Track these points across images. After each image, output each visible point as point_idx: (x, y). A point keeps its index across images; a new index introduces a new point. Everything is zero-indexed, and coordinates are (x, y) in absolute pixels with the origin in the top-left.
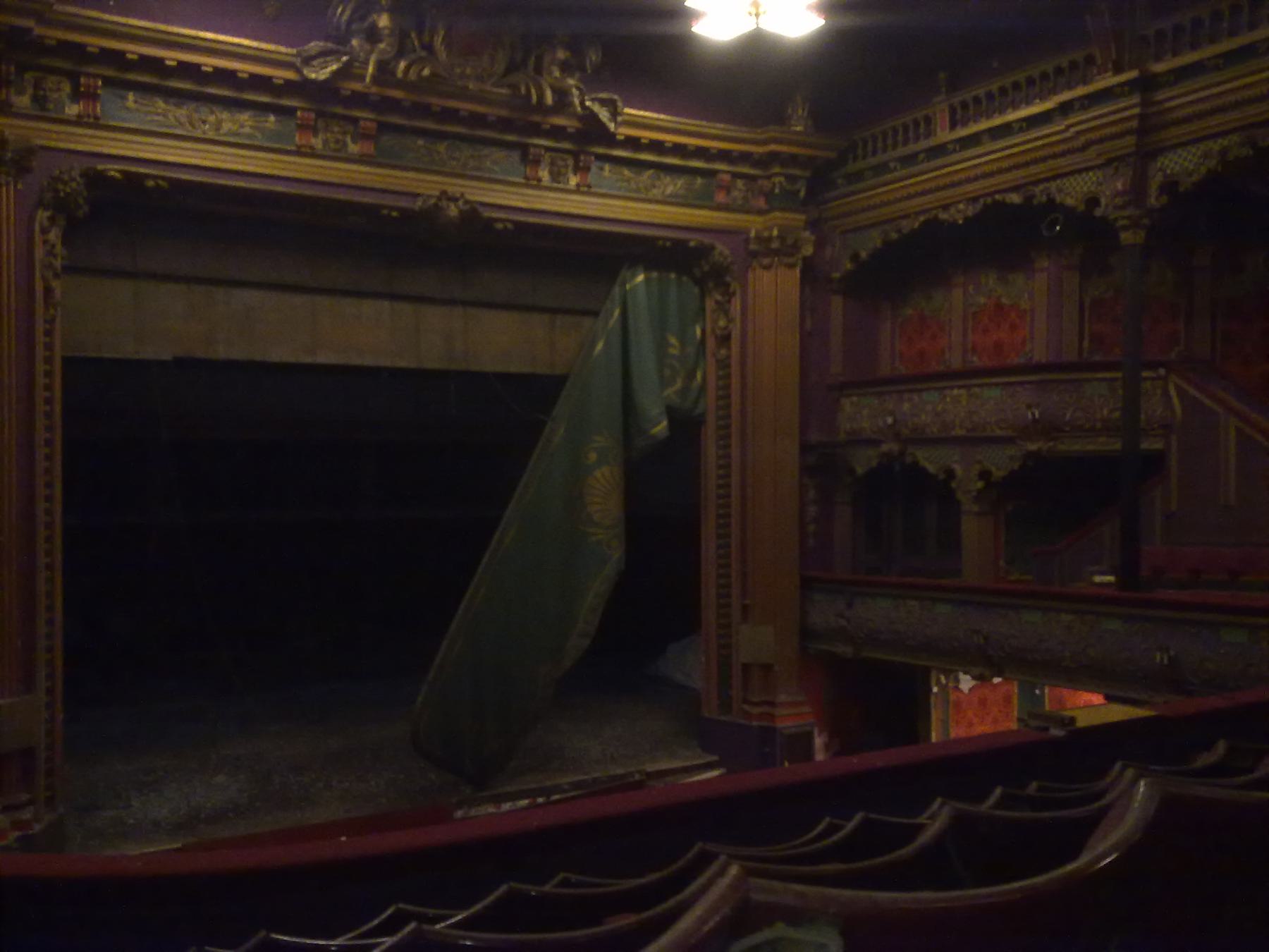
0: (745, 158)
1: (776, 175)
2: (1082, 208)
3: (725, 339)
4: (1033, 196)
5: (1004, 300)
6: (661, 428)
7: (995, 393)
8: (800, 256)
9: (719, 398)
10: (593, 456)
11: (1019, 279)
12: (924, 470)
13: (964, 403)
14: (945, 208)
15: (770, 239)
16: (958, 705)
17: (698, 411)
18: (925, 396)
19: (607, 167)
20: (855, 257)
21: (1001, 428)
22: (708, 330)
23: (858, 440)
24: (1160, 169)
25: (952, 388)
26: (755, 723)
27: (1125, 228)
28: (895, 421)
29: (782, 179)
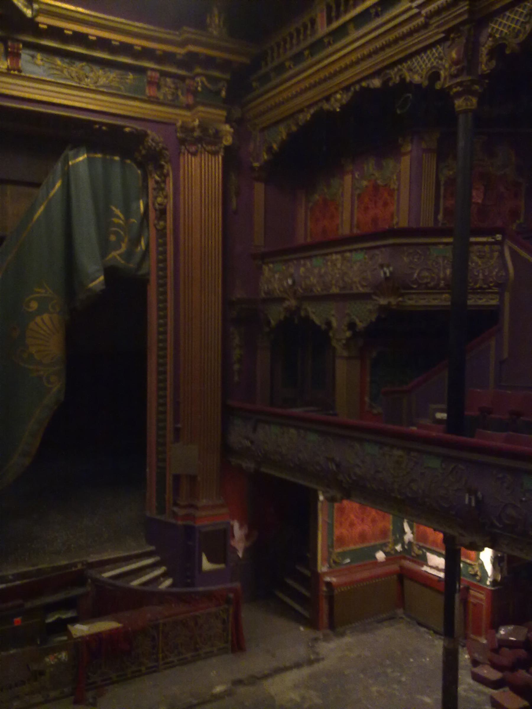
0: (166, 58)
1: (198, 75)
2: (426, 83)
3: (162, 213)
4: (390, 79)
5: (379, 182)
7: (359, 256)
8: (223, 146)
9: (159, 261)
10: (34, 305)
11: (390, 164)
12: (313, 322)
14: (327, 99)
15: (193, 130)
17: (141, 272)
18: (314, 260)
19: (39, 56)
20: (270, 149)
21: (363, 286)
24: (490, 36)
25: (331, 254)
26: (180, 523)
27: (459, 95)
28: (294, 282)
29: (204, 79)
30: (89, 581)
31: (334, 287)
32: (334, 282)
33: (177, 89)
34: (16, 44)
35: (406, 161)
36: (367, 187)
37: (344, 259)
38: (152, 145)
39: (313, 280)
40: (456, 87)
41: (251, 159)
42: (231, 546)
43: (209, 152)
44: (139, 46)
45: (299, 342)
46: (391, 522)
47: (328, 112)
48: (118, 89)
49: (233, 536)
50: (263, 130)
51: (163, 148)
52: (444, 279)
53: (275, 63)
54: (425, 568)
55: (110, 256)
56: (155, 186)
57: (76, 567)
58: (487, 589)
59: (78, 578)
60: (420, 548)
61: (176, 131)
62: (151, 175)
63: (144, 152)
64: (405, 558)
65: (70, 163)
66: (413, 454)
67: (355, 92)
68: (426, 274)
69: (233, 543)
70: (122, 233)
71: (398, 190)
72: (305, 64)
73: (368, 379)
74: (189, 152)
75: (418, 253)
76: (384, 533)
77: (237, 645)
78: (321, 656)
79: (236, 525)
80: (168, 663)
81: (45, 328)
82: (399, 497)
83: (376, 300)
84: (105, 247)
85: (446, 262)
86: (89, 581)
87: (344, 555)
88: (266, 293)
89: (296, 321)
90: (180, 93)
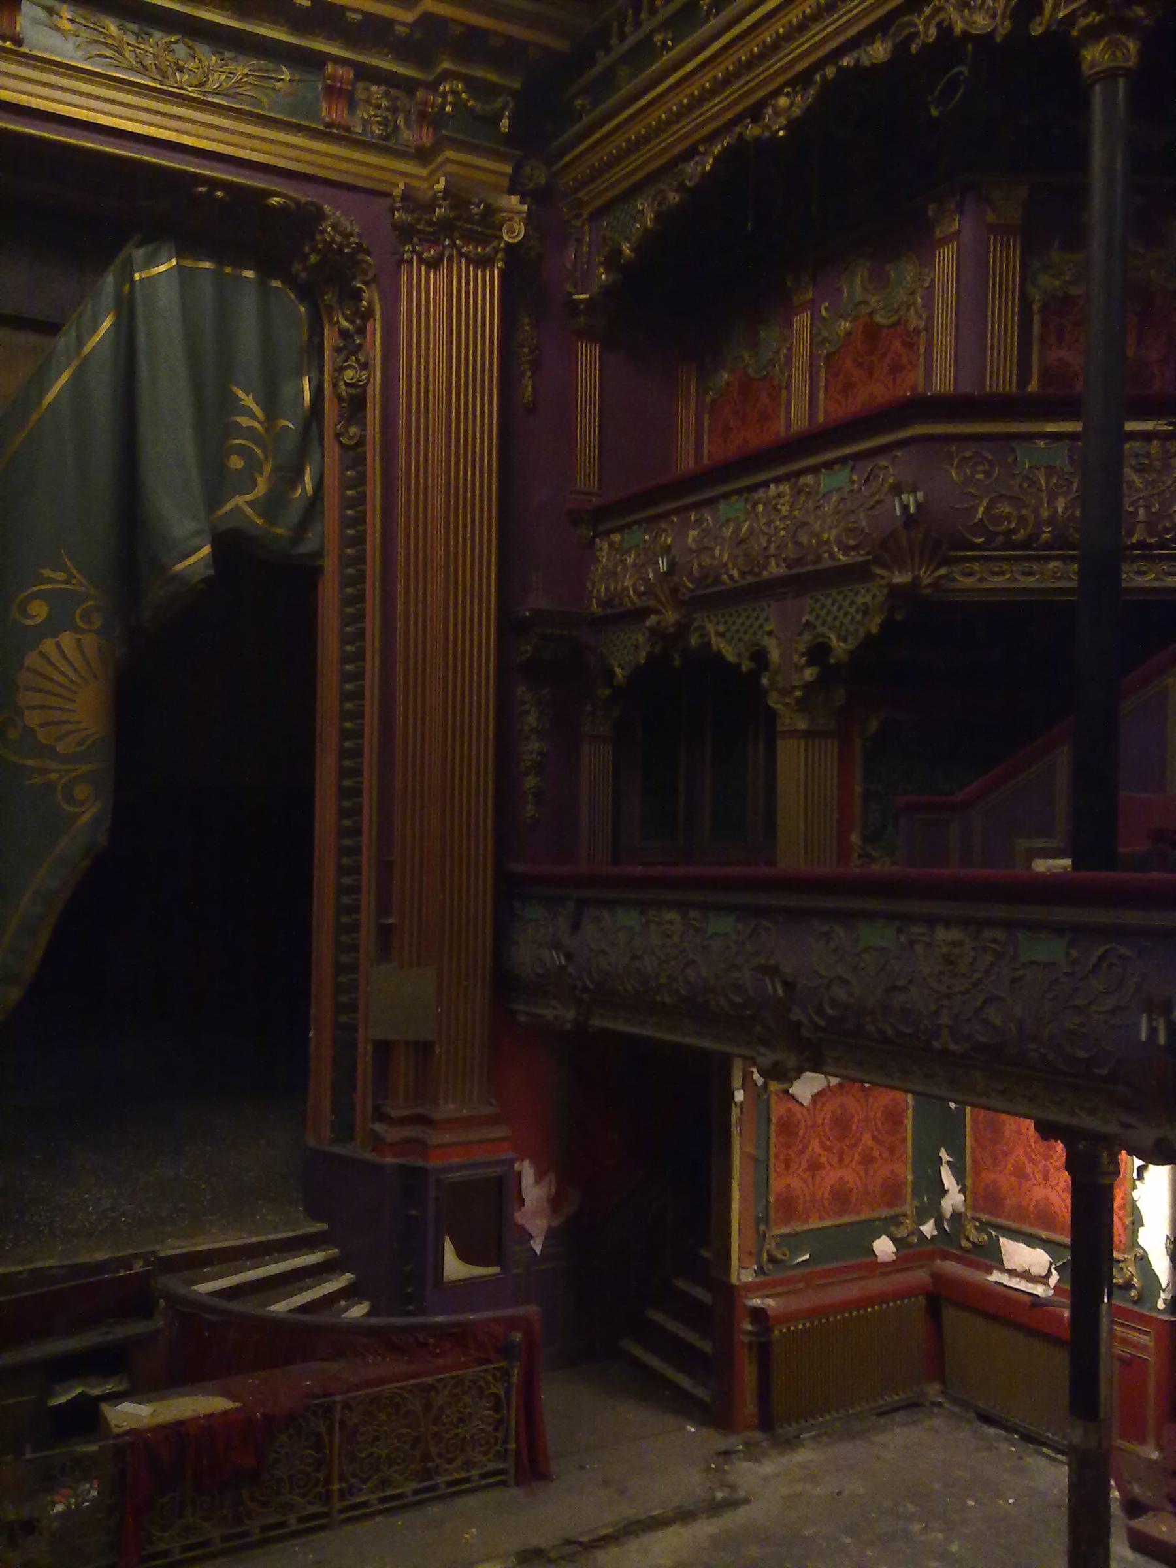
1: (446, 75)
3: (355, 405)
5: (879, 319)
6: (198, 559)
7: (839, 479)
10: (39, 611)
11: (907, 271)
13: (785, 510)
14: (755, 113)
15: (431, 206)
16: (788, 1128)
17: (303, 549)
18: (722, 506)
20: (613, 260)
21: (847, 549)
25: (765, 485)
26: (389, 1160)
27: (1094, 34)
28: (672, 565)
30: (162, 1303)
31: (773, 562)
33: (395, 110)
35: (946, 259)
36: (849, 334)
37: (798, 492)
38: (333, 241)
39: (721, 553)
40: (1085, 15)
41: (569, 287)
42: (516, 1225)
45: (688, 716)
48: (256, 102)
49: (522, 1202)
50: (595, 216)
51: (359, 248)
52: (1051, 521)
53: (631, 40)
54: (996, 1276)
55: (229, 506)
58: (1161, 1320)
59: (132, 1295)
60: (983, 1227)
61: (392, 210)
62: (331, 318)
63: (313, 259)
64: (946, 1256)
65: (137, 276)
66: (988, 934)
68: (1005, 508)
69: (519, 1217)
70: (258, 451)
71: (929, 328)
74: (421, 261)
75: (986, 458)
76: (893, 1192)
77: (531, 1467)
78: (741, 1494)
82: (953, 1047)
84: (217, 484)
86: (162, 1303)
87: (794, 1242)
88: (603, 604)
90: (401, 121)
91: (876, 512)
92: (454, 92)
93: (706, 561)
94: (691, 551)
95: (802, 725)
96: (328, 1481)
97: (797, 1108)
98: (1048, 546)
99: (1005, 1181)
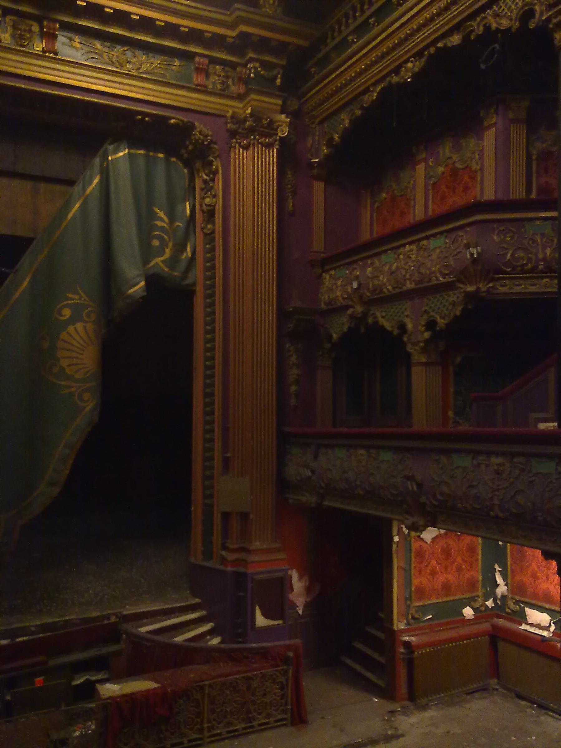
0: (217, 41)
1: (251, 60)
3: (210, 214)
5: (458, 165)
9: (207, 269)
10: (67, 313)
12: (382, 327)
14: (397, 71)
15: (245, 121)
16: (420, 554)
17: (189, 281)
18: (383, 257)
19: (77, 39)
21: (444, 275)
22: (197, 207)
23: (335, 310)
25: (404, 245)
26: (229, 569)
28: (360, 285)
31: (408, 282)
32: (408, 276)
33: (227, 77)
34: (51, 25)
35: (490, 137)
37: (419, 249)
38: (200, 139)
39: (384, 279)
40: (556, 17)
41: (309, 156)
43: (263, 146)
44: (186, 27)
45: (368, 356)
46: (480, 571)
47: (398, 84)
48: (163, 76)
49: (292, 589)
50: (321, 123)
51: (212, 142)
52: (544, 259)
55: (152, 264)
56: (203, 186)
57: (109, 619)
59: (110, 633)
60: (517, 602)
61: (226, 123)
63: (190, 147)
64: (499, 616)
65: (110, 158)
67: (430, 56)
68: (521, 254)
69: (292, 597)
70: (166, 237)
71: (481, 169)
72: (371, 34)
73: (452, 390)
74: (240, 146)
75: (510, 230)
77: (298, 718)
78: (400, 732)
79: (295, 575)
80: (214, 736)
81: (77, 338)
82: (501, 515)
83: (462, 288)
84: (147, 253)
85: (545, 240)
87: (424, 609)
88: (326, 304)
89: (363, 330)
90: (230, 82)
91: (457, 257)
92: (255, 68)
93: (376, 282)
94: (368, 277)
95: (424, 360)
96: (202, 723)
97: (423, 544)
98: (542, 272)
99: (527, 579)
